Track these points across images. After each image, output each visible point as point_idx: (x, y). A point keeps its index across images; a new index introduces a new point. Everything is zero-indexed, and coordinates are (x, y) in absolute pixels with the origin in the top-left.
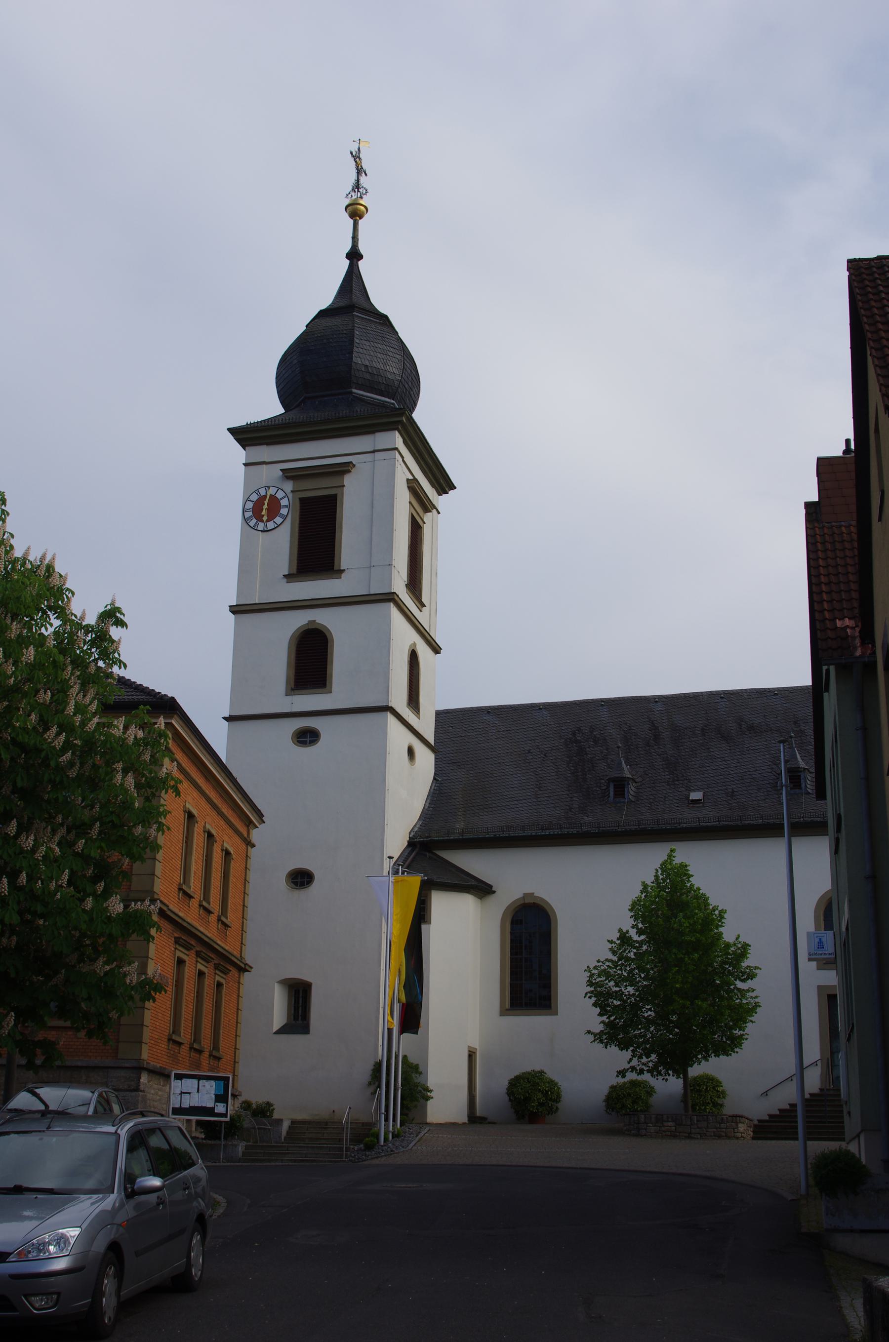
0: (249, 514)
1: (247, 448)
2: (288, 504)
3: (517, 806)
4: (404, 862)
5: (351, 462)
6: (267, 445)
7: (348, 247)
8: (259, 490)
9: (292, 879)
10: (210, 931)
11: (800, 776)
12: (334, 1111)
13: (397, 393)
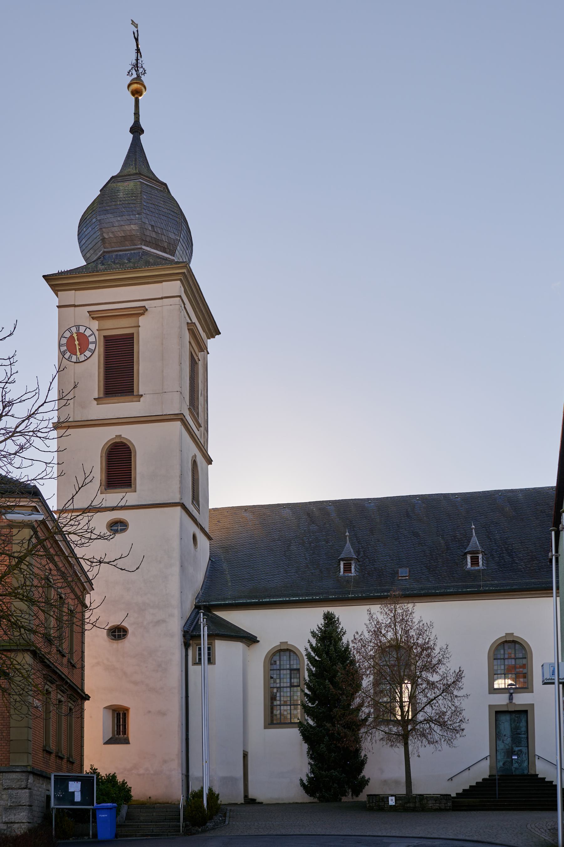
0: (64, 348)
1: (59, 293)
2: (95, 340)
3: (273, 579)
4: (193, 622)
5: (145, 306)
7: (131, 122)
8: (71, 329)
9: (111, 633)
10: (65, 671)
11: (478, 556)
12: (150, 798)
13: (177, 251)
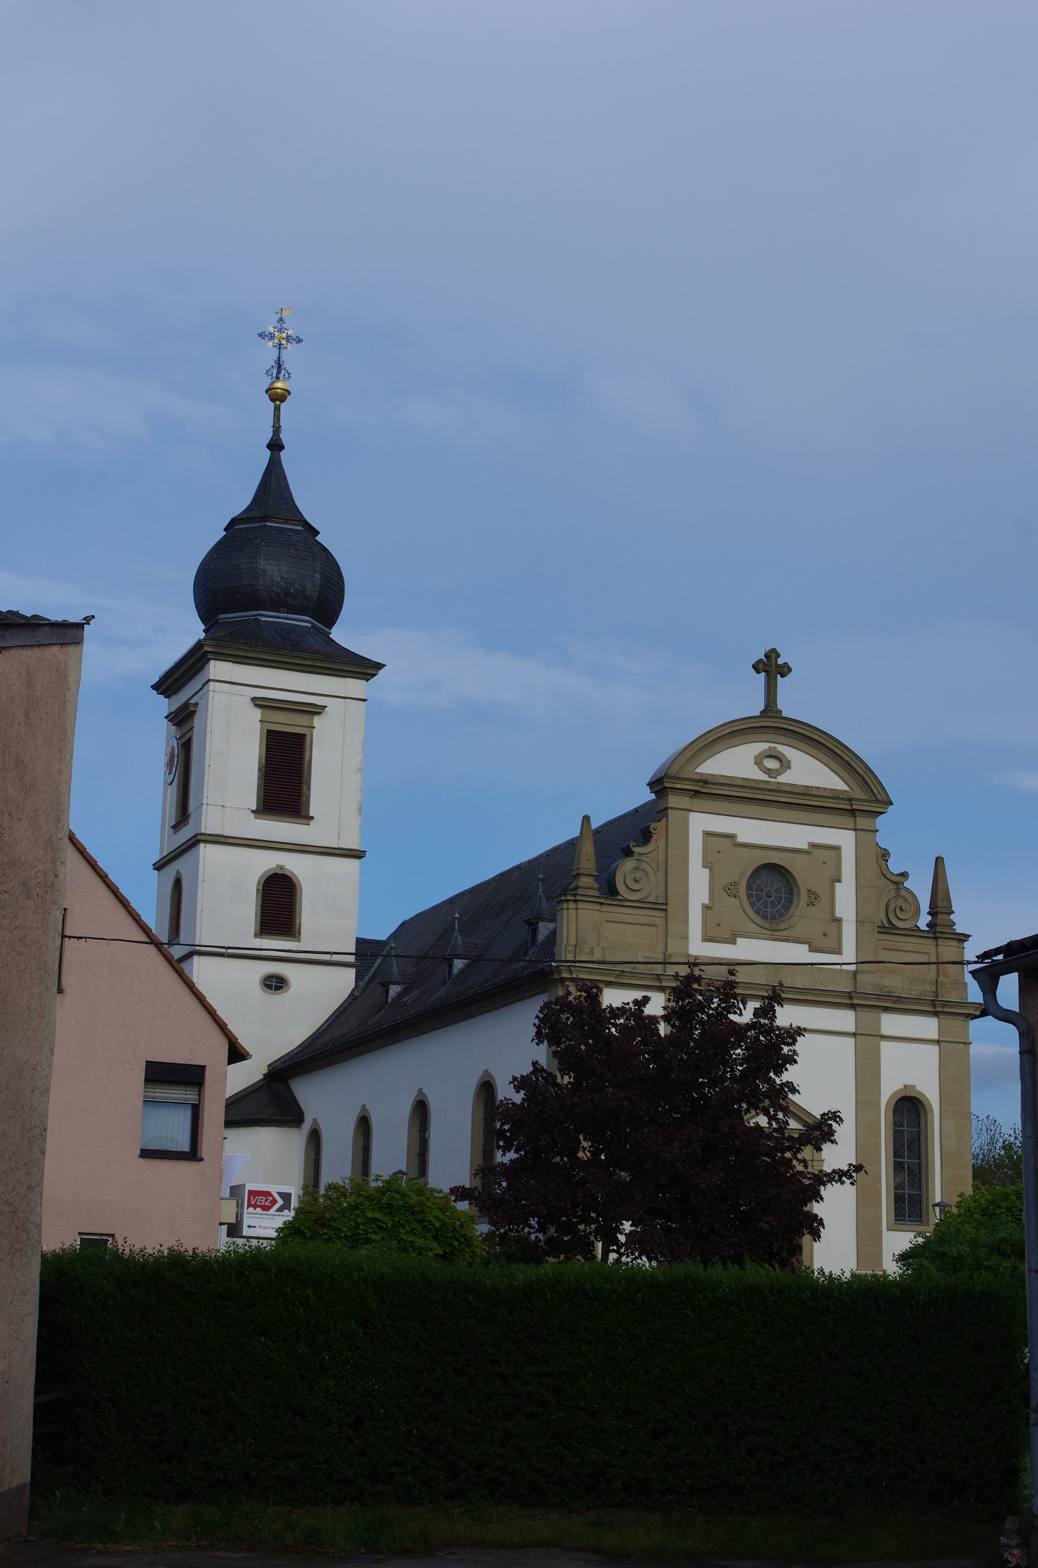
6: (175, 694)
7: (269, 435)
